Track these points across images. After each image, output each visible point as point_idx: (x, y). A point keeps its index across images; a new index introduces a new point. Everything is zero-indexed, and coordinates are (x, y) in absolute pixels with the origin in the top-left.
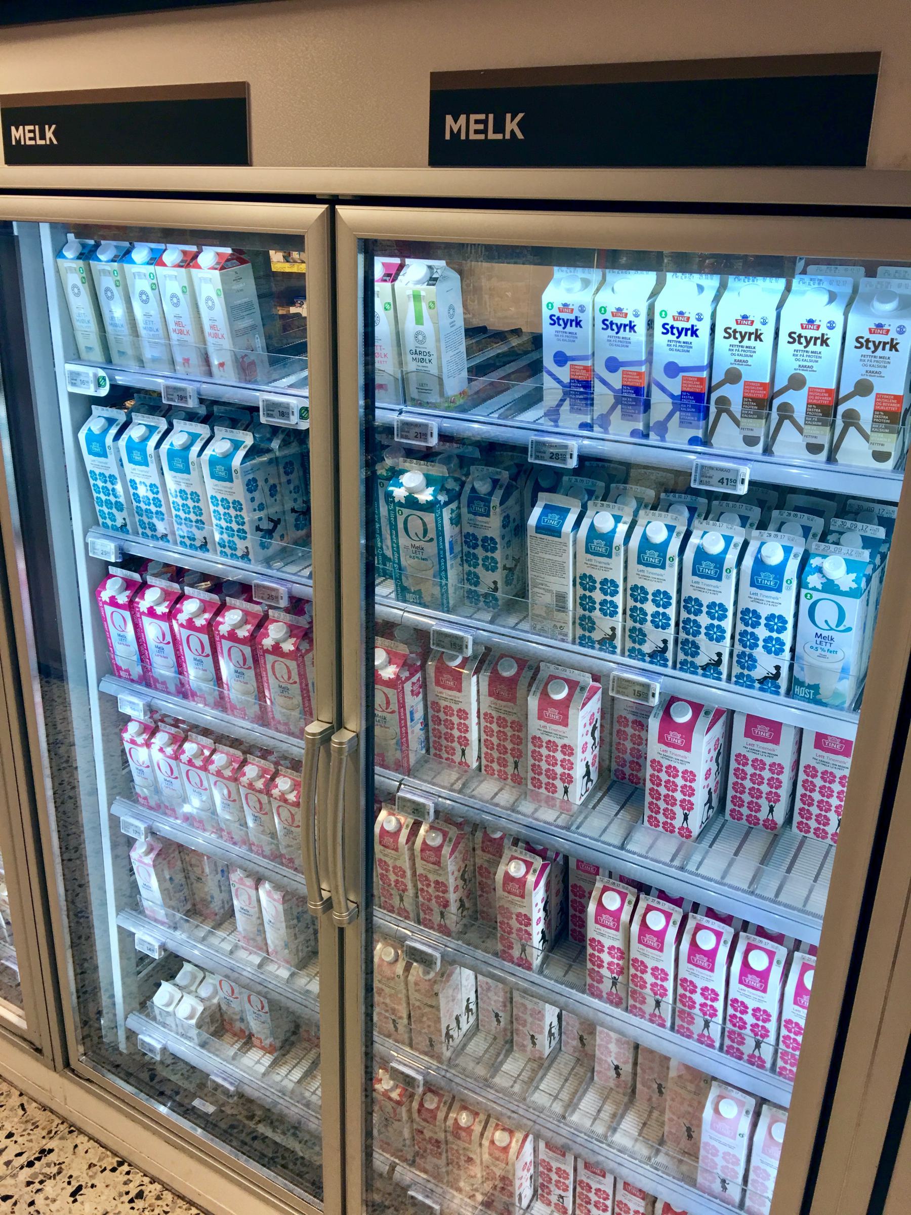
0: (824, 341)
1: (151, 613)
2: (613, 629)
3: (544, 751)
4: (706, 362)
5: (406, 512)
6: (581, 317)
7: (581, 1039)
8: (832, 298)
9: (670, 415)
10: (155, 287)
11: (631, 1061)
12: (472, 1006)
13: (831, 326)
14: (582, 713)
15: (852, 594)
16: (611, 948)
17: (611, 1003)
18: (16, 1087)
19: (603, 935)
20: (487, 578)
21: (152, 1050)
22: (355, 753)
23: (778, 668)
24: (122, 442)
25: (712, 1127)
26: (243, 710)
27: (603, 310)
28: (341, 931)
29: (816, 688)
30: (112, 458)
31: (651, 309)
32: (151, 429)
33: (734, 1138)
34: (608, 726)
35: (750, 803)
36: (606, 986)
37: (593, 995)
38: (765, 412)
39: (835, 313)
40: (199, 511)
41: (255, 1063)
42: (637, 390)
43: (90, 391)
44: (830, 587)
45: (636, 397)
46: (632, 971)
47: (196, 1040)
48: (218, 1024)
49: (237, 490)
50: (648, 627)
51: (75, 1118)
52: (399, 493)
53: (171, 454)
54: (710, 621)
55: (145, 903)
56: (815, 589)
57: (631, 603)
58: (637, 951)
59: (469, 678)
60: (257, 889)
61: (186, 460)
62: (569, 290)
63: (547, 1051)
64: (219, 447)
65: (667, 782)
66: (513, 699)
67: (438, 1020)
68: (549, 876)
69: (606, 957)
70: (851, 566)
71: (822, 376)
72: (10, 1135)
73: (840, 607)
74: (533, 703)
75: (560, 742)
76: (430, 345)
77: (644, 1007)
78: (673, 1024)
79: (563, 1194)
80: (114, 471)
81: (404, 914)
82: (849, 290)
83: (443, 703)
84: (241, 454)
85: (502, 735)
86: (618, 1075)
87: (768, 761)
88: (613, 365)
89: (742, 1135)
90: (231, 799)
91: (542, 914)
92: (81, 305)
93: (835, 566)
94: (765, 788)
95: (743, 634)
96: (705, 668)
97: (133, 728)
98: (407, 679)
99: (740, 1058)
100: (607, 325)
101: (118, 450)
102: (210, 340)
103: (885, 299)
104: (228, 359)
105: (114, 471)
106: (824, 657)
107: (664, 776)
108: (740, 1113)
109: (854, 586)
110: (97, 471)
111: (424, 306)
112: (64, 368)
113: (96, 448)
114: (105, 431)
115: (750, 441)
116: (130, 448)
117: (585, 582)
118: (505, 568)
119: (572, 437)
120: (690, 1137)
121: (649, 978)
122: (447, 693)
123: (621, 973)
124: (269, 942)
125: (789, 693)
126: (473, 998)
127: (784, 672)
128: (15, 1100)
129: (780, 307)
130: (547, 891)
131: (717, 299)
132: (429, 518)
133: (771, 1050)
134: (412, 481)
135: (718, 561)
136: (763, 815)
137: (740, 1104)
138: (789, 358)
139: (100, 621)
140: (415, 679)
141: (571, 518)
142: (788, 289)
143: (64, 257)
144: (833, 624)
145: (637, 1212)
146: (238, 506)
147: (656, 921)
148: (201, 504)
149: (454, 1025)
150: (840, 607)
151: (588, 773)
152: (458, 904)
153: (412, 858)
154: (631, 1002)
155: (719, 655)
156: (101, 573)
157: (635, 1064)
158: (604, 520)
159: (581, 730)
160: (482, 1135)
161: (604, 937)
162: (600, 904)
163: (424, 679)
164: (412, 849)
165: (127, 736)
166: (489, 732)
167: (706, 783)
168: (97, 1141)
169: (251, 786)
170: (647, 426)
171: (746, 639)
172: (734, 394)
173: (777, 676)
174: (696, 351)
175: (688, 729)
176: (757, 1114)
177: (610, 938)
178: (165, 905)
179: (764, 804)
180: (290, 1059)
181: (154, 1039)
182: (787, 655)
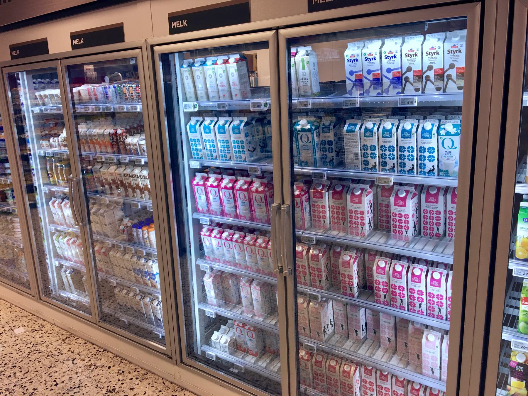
0: (438, 53)
1: (212, 186)
2: (375, 163)
3: (354, 215)
4: (400, 66)
5: (301, 133)
6: (358, 58)
7: (375, 331)
8: (439, 39)
9: (390, 86)
10: (214, 72)
11: (394, 335)
12: (332, 323)
13: (439, 48)
14: (366, 198)
15: (456, 134)
16: (383, 282)
17: (385, 305)
18: (160, 376)
19: (380, 278)
20: (330, 155)
21: (212, 357)
22: (288, 212)
23: (433, 166)
24: (202, 126)
25: (426, 346)
26: (244, 217)
27: (365, 54)
28: (285, 278)
29: (447, 171)
30: (198, 133)
31: (381, 53)
32: (212, 121)
33: (434, 349)
34: (376, 208)
35: (430, 228)
36: (382, 299)
37: (377, 303)
38: (421, 80)
39: (440, 44)
40: (228, 147)
41: (250, 360)
42: (378, 79)
43: (192, 110)
44: (448, 134)
45: (378, 81)
46: (391, 290)
47: (228, 352)
48: (235, 346)
49: (242, 137)
50: (387, 160)
51: (184, 385)
52: (299, 127)
53: (219, 128)
54: (408, 154)
55: (208, 299)
56: (443, 135)
57: (381, 152)
58: (393, 281)
59: (325, 193)
60: (250, 287)
61: (224, 129)
62: (353, 50)
63: (362, 337)
64: (236, 122)
65: (399, 220)
66: (341, 198)
67: (321, 324)
68: (358, 261)
69: (381, 287)
70: (454, 126)
71: (438, 65)
72: (160, 391)
73: (452, 140)
74: (349, 197)
75: (359, 210)
76: (308, 76)
77: (397, 304)
78: (408, 309)
79: (372, 393)
80: (199, 137)
81: (305, 284)
82: (444, 37)
83: (316, 204)
84: (243, 124)
85: (338, 213)
86: (390, 342)
87: (435, 210)
88: (369, 72)
89: (437, 347)
90: (241, 250)
91: (356, 275)
92: (188, 83)
93: (449, 126)
94: (435, 221)
95: (421, 156)
96: (408, 171)
97: (204, 230)
98: (303, 195)
99: (434, 317)
100: (367, 59)
101: (200, 130)
102: (232, 87)
103: (455, 37)
104: (238, 92)
105: (199, 137)
106: (449, 159)
107: (397, 218)
108: (436, 339)
109: (456, 132)
110: (193, 139)
111: (305, 63)
112: (182, 104)
113: (193, 130)
114: (196, 124)
115: (417, 90)
116: (205, 128)
117: (364, 147)
118: (336, 151)
119: (357, 98)
120: (419, 358)
121: (398, 291)
122: (317, 200)
123: (387, 292)
124: (255, 308)
125: (438, 175)
126: (332, 320)
127: (436, 168)
128: (160, 381)
129: (422, 44)
130: (358, 267)
131: (401, 46)
132: (310, 135)
133: (445, 311)
134: (303, 123)
135: (410, 132)
136: (435, 232)
137: (436, 336)
138: (427, 61)
139: (193, 191)
140: (306, 196)
141: (358, 127)
142: (425, 39)
143: (183, 67)
144: (450, 147)
145: (401, 394)
146: (242, 142)
147: (399, 268)
148: (229, 144)
149: (326, 327)
150: (452, 140)
151: (370, 223)
152: (325, 277)
153: (308, 261)
154: (392, 303)
155: (413, 165)
156: (194, 172)
157: (396, 337)
158: (370, 125)
159: (366, 205)
160: (340, 369)
161: (379, 278)
162: (378, 265)
163: (319, 131)
164: (308, 257)
165: (202, 233)
166: (333, 212)
167: (413, 219)
168: (192, 393)
169: (248, 244)
170: (382, 92)
171: (421, 158)
172: (410, 75)
173: (433, 169)
174: (396, 64)
175: (404, 199)
176: (442, 338)
177: (382, 278)
178: (216, 298)
179: (435, 227)
180: (265, 358)
181: (212, 353)
182: (436, 161)
